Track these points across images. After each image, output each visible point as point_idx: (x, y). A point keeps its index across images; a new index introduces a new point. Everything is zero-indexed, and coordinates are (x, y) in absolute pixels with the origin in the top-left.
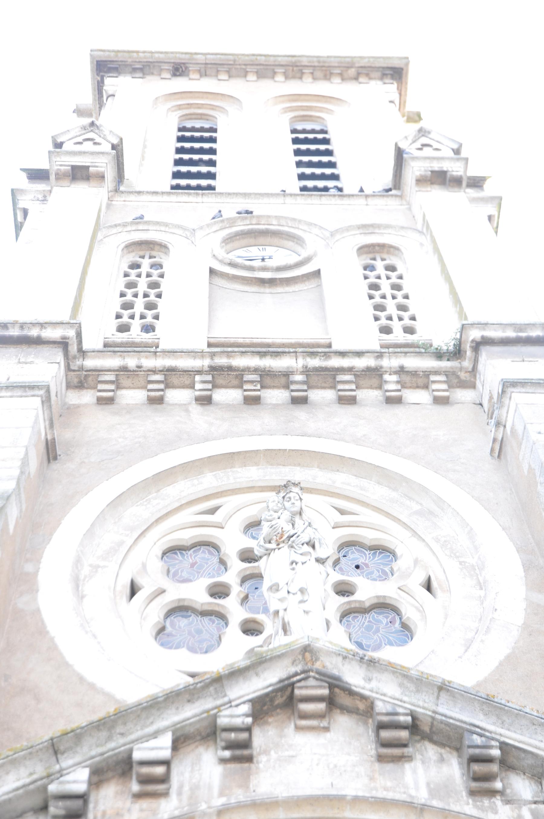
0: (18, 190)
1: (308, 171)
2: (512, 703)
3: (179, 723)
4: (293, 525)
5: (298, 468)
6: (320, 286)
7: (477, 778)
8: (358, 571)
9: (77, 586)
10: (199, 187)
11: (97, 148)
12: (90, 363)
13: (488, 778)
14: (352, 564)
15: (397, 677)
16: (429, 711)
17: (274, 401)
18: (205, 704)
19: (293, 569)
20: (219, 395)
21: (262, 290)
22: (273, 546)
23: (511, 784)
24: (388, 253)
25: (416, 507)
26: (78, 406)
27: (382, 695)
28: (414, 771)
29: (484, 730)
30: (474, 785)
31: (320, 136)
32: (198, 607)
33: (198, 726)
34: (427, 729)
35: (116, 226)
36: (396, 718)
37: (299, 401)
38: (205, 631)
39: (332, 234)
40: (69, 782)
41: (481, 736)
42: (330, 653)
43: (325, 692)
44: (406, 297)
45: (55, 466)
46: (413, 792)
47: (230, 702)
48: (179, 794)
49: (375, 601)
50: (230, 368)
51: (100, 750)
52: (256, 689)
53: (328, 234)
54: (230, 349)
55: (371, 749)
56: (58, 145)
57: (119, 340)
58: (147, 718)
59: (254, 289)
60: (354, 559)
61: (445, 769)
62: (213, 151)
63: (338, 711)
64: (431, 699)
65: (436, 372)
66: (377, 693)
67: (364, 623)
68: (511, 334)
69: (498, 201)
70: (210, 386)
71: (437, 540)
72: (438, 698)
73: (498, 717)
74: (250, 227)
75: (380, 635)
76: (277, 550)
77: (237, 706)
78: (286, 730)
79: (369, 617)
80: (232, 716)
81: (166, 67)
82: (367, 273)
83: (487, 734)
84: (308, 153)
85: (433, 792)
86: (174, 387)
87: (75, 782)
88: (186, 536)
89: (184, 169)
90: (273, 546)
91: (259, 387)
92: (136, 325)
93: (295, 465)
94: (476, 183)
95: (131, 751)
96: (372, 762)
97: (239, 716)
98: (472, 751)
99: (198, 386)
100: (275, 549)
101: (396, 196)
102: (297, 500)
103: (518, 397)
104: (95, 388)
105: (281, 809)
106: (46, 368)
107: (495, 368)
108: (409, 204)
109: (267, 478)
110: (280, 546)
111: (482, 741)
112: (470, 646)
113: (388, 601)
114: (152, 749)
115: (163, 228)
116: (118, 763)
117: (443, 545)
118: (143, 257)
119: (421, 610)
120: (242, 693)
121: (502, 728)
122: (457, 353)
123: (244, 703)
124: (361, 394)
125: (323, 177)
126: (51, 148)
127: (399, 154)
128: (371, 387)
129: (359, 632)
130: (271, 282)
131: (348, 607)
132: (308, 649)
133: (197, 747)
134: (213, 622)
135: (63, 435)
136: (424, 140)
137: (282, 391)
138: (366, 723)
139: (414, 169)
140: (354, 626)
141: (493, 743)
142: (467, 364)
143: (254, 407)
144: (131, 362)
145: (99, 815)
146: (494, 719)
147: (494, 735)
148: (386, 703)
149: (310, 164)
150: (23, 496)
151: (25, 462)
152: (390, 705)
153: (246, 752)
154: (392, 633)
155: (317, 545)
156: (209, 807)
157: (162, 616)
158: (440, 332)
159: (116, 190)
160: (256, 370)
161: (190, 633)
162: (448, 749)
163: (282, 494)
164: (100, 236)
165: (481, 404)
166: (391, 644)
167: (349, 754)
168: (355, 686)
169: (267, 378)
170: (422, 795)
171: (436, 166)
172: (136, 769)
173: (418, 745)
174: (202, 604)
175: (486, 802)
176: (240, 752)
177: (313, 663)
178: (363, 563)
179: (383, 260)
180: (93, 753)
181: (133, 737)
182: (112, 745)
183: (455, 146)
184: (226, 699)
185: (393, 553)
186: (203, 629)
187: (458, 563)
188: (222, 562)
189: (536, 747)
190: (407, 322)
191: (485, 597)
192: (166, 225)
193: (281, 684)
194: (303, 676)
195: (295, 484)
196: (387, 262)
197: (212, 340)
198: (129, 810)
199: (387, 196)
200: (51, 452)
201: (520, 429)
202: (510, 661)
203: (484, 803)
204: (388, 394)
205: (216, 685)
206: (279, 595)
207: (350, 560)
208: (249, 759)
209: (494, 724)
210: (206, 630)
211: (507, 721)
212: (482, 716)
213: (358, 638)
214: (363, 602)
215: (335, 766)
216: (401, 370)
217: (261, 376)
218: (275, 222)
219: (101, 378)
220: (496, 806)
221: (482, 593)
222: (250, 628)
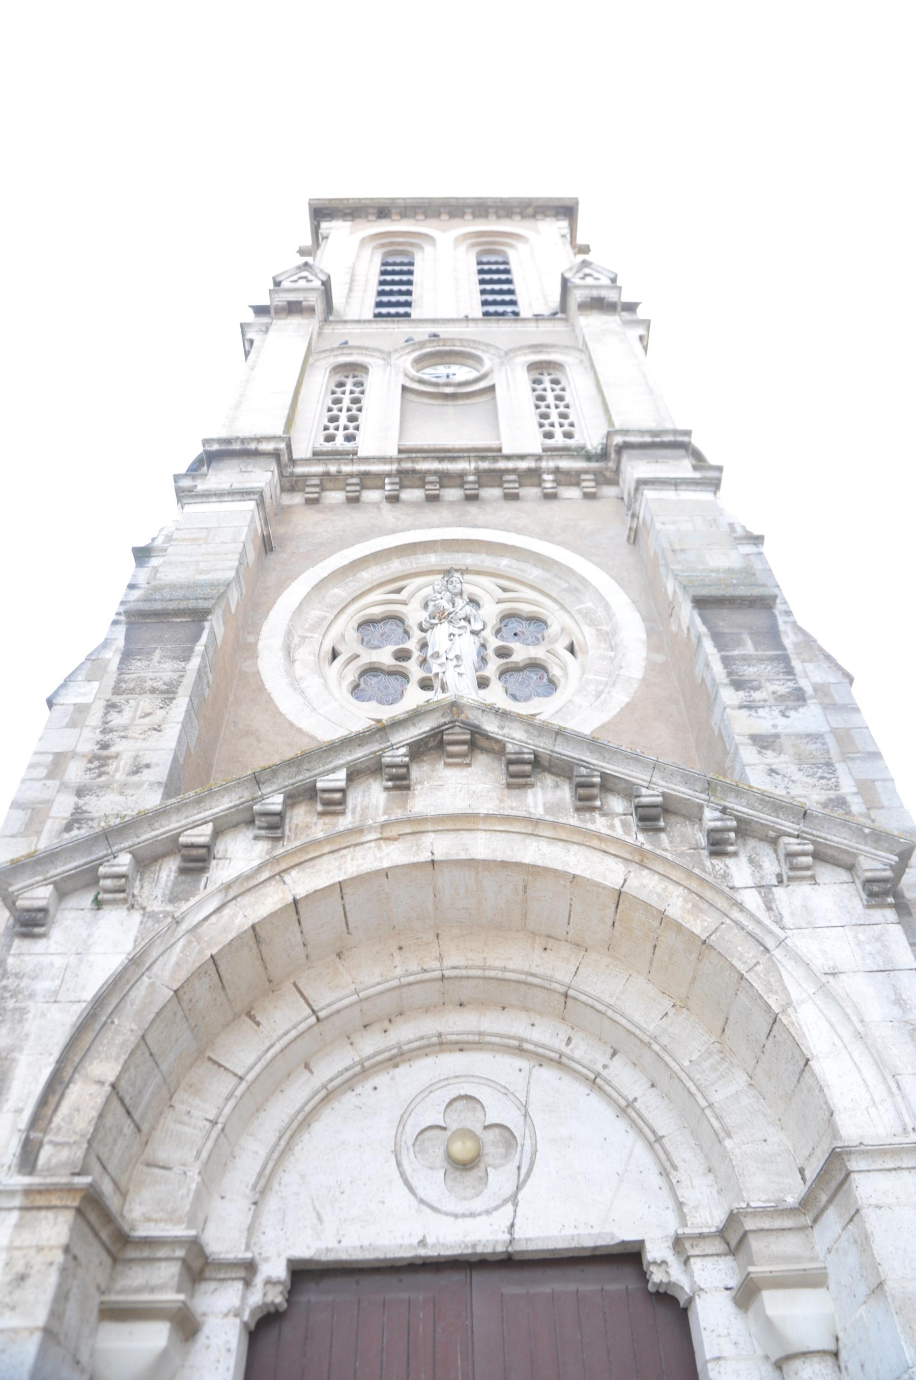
0: (245, 324)
1: (490, 298)
4: (453, 604)
6: (494, 398)
8: (516, 638)
9: (289, 653)
10: (397, 315)
11: (310, 285)
12: (299, 470)
13: (591, 798)
17: (451, 499)
18: (374, 747)
19: (451, 640)
20: (406, 495)
21: (446, 403)
22: (436, 621)
24: (554, 368)
25: (566, 585)
26: (290, 507)
28: (535, 795)
29: (590, 763)
30: (579, 804)
31: (502, 267)
32: (385, 668)
33: (367, 764)
34: (546, 764)
35: (325, 351)
36: (522, 756)
37: (472, 498)
39: (507, 353)
40: (268, 804)
42: (472, 708)
43: (468, 737)
44: (567, 406)
45: (271, 556)
46: (532, 810)
47: (392, 745)
48: (353, 812)
49: (528, 662)
50: (414, 471)
51: (292, 781)
53: (503, 353)
54: (414, 455)
56: (277, 284)
57: (325, 449)
58: (327, 758)
59: (439, 402)
61: (559, 793)
62: (410, 283)
65: (586, 472)
68: (648, 439)
69: (647, 323)
70: (397, 487)
71: (579, 611)
73: (601, 753)
74: (438, 348)
79: (522, 675)
81: (371, 211)
82: (536, 386)
84: (491, 282)
85: (547, 810)
86: (369, 488)
87: (273, 804)
88: (377, 611)
89: (385, 299)
91: (438, 487)
92: (340, 435)
93: (467, 552)
94: (631, 307)
95: (315, 781)
97: (399, 756)
98: (578, 779)
99: (387, 487)
101: (562, 319)
103: (649, 494)
104: (303, 490)
106: (262, 477)
107: (636, 468)
108: (573, 325)
113: (538, 662)
114: (332, 780)
115: (364, 352)
116: (306, 791)
118: (347, 377)
119: (564, 668)
120: (401, 739)
122: (603, 455)
123: (403, 746)
124: (523, 492)
125: (503, 303)
126: (272, 287)
127: (565, 282)
128: (532, 485)
130: (454, 396)
134: (398, 680)
135: (278, 530)
136: (587, 271)
137: (458, 489)
138: (500, 760)
139: (577, 296)
141: (596, 773)
142: (611, 465)
143: (435, 503)
144: (333, 469)
145: (293, 827)
146: (598, 755)
149: (493, 292)
150: (242, 582)
151: (243, 554)
153: (405, 783)
155: (472, 620)
157: (357, 676)
158: (591, 436)
159: (326, 320)
160: (435, 472)
161: (379, 689)
163: (446, 579)
164: (311, 360)
165: (622, 499)
166: (539, 696)
169: (445, 479)
170: (539, 811)
171: (595, 293)
172: (319, 794)
173: (539, 776)
175: (588, 816)
176: (400, 782)
179: (549, 374)
180: (286, 784)
181: (316, 772)
182: (301, 777)
183: (612, 276)
184: (389, 744)
185: (545, 622)
188: (406, 632)
190: (567, 428)
191: (615, 657)
192: (367, 349)
195: (457, 571)
196: (553, 377)
197: (402, 447)
198: (315, 824)
199: (555, 319)
200: (267, 545)
201: (648, 520)
202: (629, 708)
204: (545, 491)
205: (382, 733)
206: (439, 661)
208: (408, 788)
209: (597, 759)
212: (588, 754)
216: (557, 471)
217: (440, 478)
218: (458, 344)
219: (308, 483)
221: (612, 654)
222: (426, 685)
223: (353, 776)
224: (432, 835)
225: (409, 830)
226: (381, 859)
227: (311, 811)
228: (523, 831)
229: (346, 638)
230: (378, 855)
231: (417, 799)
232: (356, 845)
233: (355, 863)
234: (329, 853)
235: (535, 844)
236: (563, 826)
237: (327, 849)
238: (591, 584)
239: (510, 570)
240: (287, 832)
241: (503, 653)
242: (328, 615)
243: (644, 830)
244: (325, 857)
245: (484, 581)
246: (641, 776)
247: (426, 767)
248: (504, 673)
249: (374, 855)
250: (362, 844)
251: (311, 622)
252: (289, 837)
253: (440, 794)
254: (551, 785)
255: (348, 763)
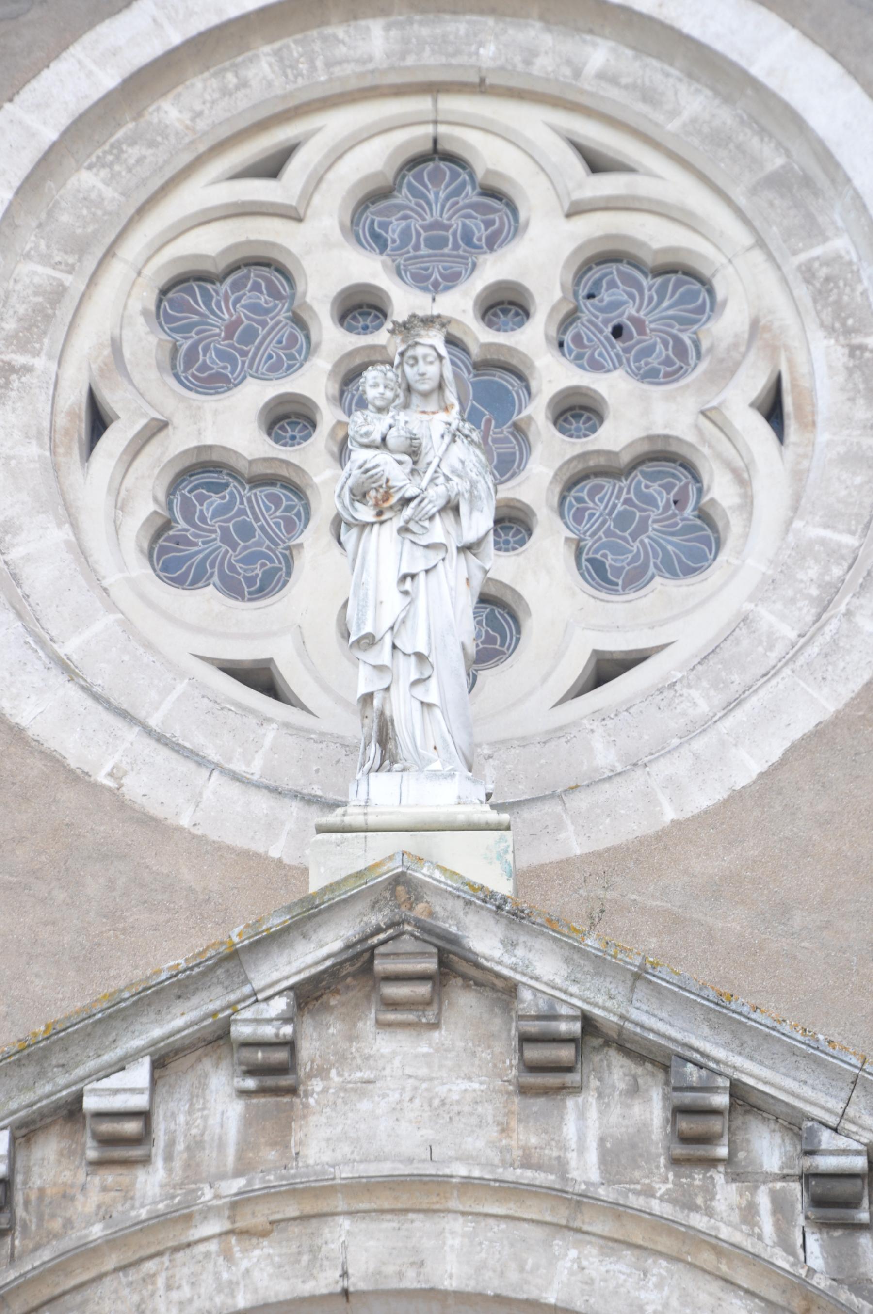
2: (762, 1012)
3: (162, 1039)
5: (491, 21)
7: (686, 1139)
8: (619, 345)
13: (706, 1139)
14: (606, 322)
15: (561, 948)
16: (615, 1014)
19: (406, 593)
23: (748, 1141)
27: (531, 978)
28: (582, 1115)
30: (680, 1150)
32: (241, 466)
36: (553, 1025)
38: (258, 531)
41: (701, 1068)
43: (430, 965)
49: (645, 448)
52: (302, 966)
55: (511, 1066)
60: (615, 305)
61: (637, 1109)
63: (460, 981)
64: (621, 989)
66: (524, 974)
67: (615, 506)
72: (632, 989)
75: (646, 541)
76: (376, 527)
77: (268, 999)
78: (360, 1025)
80: (258, 1021)
83: (712, 1065)
88: (211, 243)
90: (366, 513)
96: (509, 1093)
97: (269, 1021)
100: (373, 524)
102: (431, 363)
105: (339, 1195)
109: (410, 61)
110: (384, 518)
111: (700, 1077)
112: (830, 602)
113: (674, 448)
114: (116, 1092)
117: (820, 292)
120: (275, 976)
121: (740, 1054)
123: (279, 993)
129: (601, 533)
131: (580, 466)
132: (402, 880)
133: (199, 1060)
140: (592, 515)
145: (33, 1197)
146: (727, 1037)
147: (722, 1068)
148: (539, 995)
152: (546, 997)
153: (285, 1081)
154: (673, 534)
156: (217, 1196)
161: (226, 537)
162: (649, 1066)
167: (470, 1079)
168: (487, 959)
174: (251, 462)
176: (275, 1075)
177: (411, 904)
178: (631, 319)
181: (80, 1072)
182: (48, 1088)
184: (247, 990)
186: (255, 525)
187: (846, 351)
189: (793, 1094)
193: (351, 952)
194: (390, 932)
198: (83, 1188)
203: (694, 1179)
207: (602, 310)
208: (292, 1091)
209: (726, 1046)
210: (262, 528)
211: (749, 1042)
212: (706, 1031)
213: (596, 551)
214: (616, 454)
215: (443, 1103)
220: (714, 1186)
223: (164, 1061)
224: (345, 1223)
225: (292, 1211)
226: (231, 1287)
227: (72, 1153)
228: (548, 1218)
229: (127, 353)
230: (225, 1276)
231: (313, 1119)
232: (176, 1249)
233: (175, 1295)
234: (116, 1270)
235: (573, 1253)
236: (639, 1216)
237: (112, 1261)
238: (848, 180)
239: (613, 93)
240: (20, 1212)
241: (577, 411)
242: (68, 280)
243: (825, 1225)
244: (107, 1280)
245: (534, 122)
246: (822, 1099)
247: (335, 1028)
248: (578, 479)
249: (217, 1275)
250: (189, 1245)
251: (22, 310)
252: (25, 1227)
253: (365, 1105)
254: (621, 1085)
255: (155, 1043)
